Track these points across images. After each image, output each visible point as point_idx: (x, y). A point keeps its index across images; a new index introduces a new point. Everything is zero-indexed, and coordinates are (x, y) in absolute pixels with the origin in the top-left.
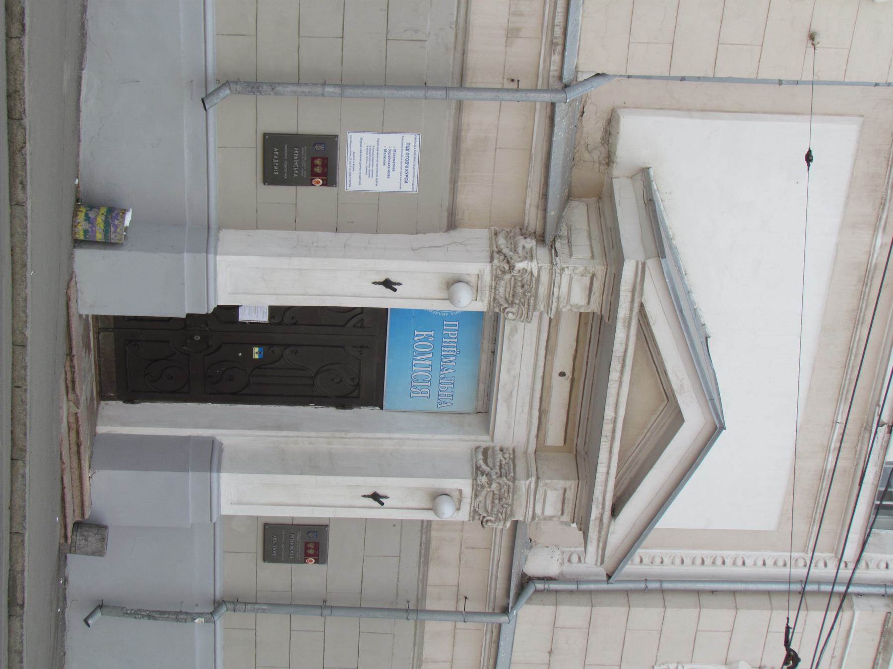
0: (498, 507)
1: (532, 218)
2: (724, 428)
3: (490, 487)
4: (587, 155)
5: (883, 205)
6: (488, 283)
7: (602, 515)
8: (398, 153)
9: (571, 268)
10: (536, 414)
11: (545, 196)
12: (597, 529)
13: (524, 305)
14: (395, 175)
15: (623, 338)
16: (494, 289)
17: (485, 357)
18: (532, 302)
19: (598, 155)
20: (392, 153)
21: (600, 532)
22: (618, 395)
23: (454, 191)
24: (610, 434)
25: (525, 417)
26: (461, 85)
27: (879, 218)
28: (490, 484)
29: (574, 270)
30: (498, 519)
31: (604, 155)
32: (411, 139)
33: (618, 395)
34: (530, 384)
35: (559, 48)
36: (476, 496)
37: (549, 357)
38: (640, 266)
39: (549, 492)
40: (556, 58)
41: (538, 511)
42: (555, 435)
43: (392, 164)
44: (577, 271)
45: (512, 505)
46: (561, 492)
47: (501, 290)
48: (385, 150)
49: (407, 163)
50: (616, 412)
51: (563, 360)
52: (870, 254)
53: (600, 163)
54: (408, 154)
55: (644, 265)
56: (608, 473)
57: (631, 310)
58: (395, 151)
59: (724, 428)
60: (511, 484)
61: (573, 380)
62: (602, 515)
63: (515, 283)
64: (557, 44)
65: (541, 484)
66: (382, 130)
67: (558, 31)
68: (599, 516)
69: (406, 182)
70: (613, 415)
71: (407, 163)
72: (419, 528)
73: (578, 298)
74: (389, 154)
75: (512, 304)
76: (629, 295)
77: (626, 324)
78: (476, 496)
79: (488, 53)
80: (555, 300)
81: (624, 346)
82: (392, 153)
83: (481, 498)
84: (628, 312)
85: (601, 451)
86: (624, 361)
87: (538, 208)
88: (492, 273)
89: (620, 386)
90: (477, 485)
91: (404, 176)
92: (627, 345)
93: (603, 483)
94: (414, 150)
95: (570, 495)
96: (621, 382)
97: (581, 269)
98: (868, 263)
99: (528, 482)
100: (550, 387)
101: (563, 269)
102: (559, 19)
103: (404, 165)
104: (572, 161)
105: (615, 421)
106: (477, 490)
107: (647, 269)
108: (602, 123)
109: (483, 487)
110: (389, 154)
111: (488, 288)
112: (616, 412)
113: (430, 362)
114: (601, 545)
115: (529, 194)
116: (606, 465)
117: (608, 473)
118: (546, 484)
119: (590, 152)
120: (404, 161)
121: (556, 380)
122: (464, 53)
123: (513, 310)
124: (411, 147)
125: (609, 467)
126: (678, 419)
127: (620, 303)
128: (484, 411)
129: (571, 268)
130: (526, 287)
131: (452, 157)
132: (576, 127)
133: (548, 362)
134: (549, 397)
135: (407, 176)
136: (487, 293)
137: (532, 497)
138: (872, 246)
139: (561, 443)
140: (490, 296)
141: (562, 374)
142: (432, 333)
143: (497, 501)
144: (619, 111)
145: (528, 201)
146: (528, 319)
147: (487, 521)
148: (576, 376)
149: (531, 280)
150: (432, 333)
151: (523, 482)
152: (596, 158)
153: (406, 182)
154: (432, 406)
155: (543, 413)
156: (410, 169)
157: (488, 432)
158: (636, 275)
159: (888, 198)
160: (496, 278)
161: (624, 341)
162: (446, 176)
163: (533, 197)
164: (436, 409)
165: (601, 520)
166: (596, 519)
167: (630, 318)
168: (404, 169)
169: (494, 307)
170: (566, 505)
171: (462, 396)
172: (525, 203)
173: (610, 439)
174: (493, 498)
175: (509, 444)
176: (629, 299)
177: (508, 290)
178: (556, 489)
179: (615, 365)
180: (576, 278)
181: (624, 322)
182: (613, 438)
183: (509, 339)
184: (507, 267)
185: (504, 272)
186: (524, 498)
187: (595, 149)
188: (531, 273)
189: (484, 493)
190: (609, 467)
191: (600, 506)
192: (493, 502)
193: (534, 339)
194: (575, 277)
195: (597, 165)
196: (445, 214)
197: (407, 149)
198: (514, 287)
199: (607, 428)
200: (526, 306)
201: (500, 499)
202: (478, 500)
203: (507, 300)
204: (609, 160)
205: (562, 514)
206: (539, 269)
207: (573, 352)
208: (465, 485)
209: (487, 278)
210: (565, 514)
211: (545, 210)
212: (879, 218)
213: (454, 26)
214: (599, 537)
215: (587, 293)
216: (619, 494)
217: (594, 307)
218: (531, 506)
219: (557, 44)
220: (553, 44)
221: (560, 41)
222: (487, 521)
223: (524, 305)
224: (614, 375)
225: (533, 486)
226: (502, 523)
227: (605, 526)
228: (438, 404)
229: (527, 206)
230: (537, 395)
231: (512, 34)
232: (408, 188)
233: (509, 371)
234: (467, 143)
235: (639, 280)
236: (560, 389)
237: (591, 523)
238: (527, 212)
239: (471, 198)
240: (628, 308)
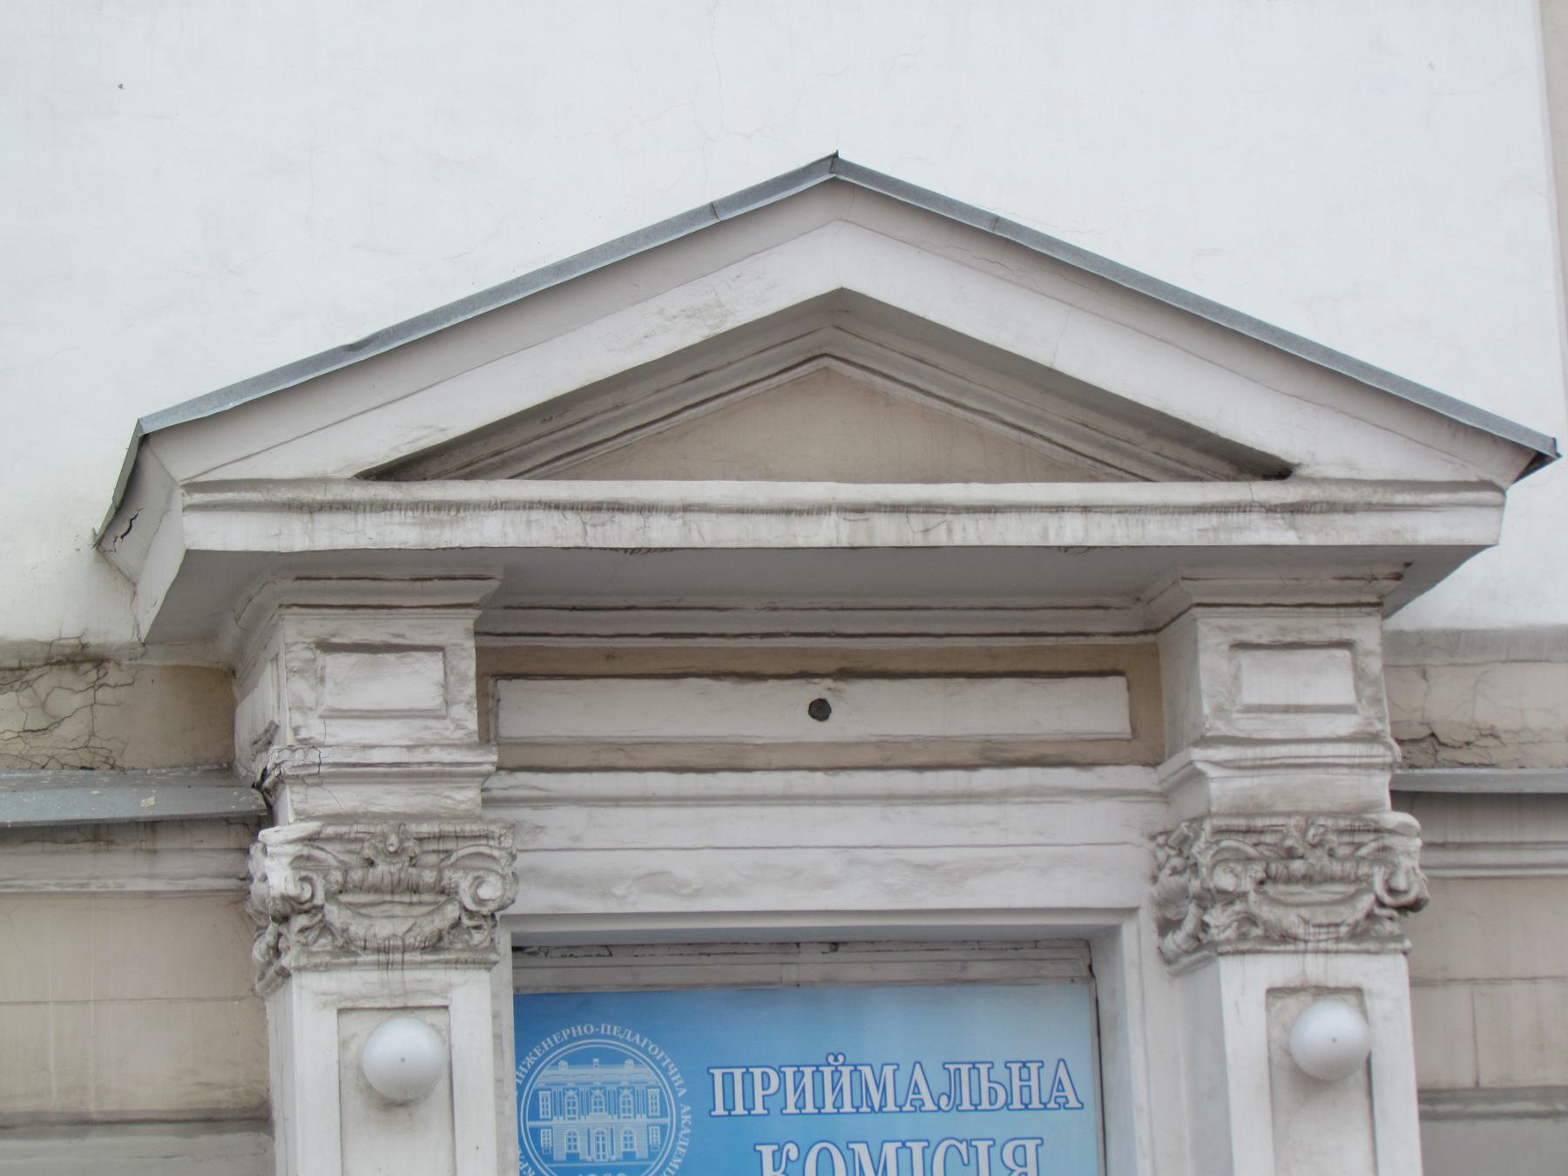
0: (1318, 859)
1: (189, 867)
2: (836, 156)
3: (1243, 896)
4: (68, 730)
6: (374, 976)
7: (1271, 509)
9: (298, 719)
10: (987, 779)
11: (98, 834)
12: (1341, 519)
13: (448, 853)
15: (504, 519)
16: (387, 953)
17: (853, 967)
18: (426, 828)
19: (67, 696)
21: (1349, 509)
22: (742, 511)
24: (916, 521)
25: (1015, 813)
28: (1229, 898)
29: (301, 708)
30: (1384, 855)
31: (67, 677)
33: (742, 511)
34: (875, 811)
36: (1286, 937)
37: (760, 758)
38: (198, 498)
39: (1250, 697)
41: (1344, 725)
42: (1097, 708)
44: (309, 700)
45: (1310, 818)
46: (1245, 658)
50: (821, 510)
51: (775, 714)
53: (98, 685)
55: (192, 487)
56: (1086, 509)
57: (385, 506)
59: (836, 156)
60: (1208, 826)
61: (846, 674)
62: (1271, 509)
63: (359, 888)
65: (1222, 728)
68: (1279, 519)
70: (831, 520)
72: (1547, 1124)
73: (414, 683)
75: (446, 892)
76: (324, 520)
77: (444, 516)
78: (1286, 937)
80: (418, 756)
81: (536, 515)
83: (1290, 920)
84: (397, 517)
85: (995, 540)
86: (596, 507)
87: (154, 852)
88: (328, 967)
89: (705, 509)
90: (1243, 937)
92: (530, 505)
93: (1133, 519)
95: (1260, 627)
96: (687, 508)
97: (300, 687)
99: (1212, 772)
100: (881, 744)
101: (308, 744)
105: (859, 509)
106: (1267, 938)
109: (1251, 920)
111: (394, 976)
112: (821, 510)
113: (890, 1149)
114: (1407, 498)
115: (112, 885)
116: (1052, 521)
117: (1086, 509)
118: (1220, 711)
119: (58, 722)
121: (840, 728)
123: (465, 885)
125: (1059, 509)
126: (841, 307)
127: (363, 543)
128: (1070, 954)
129: (298, 719)
130: (368, 852)
133: (777, 759)
134: (925, 742)
136: (411, 975)
137: (1271, 751)
139: (1115, 687)
140: (422, 965)
141: (820, 710)
142: (767, 1151)
143: (1297, 866)
145: (142, 885)
147: (1392, 891)
148: (833, 666)
149: (339, 838)
150: (767, 1151)
151: (1214, 788)
152: (77, 701)
154: (1078, 1127)
155: (995, 755)
157: (1112, 933)
158: (243, 507)
160: (347, 950)
161: (521, 516)
163: (122, 870)
164: (1091, 1113)
165: (1295, 509)
166: (1293, 527)
167: (416, 506)
170: (1307, 637)
171: (1013, 1033)
172: (151, 895)
173: (933, 519)
174: (1290, 880)
175: (1138, 857)
176: (342, 520)
177: (398, 910)
178: (1236, 677)
179: (622, 533)
181: (441, 523)
182: (929, 508)
183: (696, 894)
184: (301, 921)
185: (326, 928)
186: (1280, 778)
187: (43, 706)
188: (311, 839)
189: (1267, 912)
190: (1059, 509)
191: (1235, 519)
192: (1307, 879)
193: (687, 813)
194: (330, 701)
198: (376, 889)
199: (887, 532)
200: (450, 845)
201: (1291, 854)
202: (1300, 931)
204: (79, 658)
205: (1346, 645)
207: (726, 686)
208: (1243, 983)
209: (354, 981)
210: (1346, 635)
211: (152, 826)
214: (1370, 507)
215: (390, 657)
216: (1227, 469)
217: (457, 633)
218: (1328, 749)
222: (1392, 891)
223: (448, 853)
224: (663, 533)
225: (1225, 753)
226: (1390, 840)
227: (1314, 493)
228: (1063, 1106)
229: (158, 886)
230: (819, 782)
233: (829, 883)
235: (254, 496)
236: (868, 712)
237: (1312, 540)
238: (182, 885)
240: (383, 517)
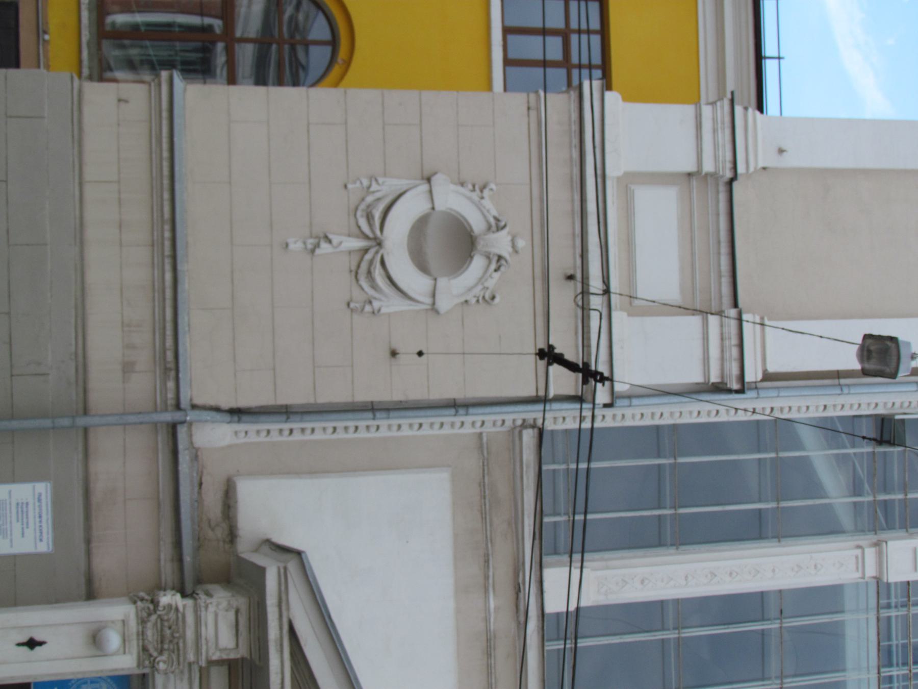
1: (168, 571)
5: (487, 562)
8: (31, 507)
9: (215, 604)
14: (29, 532)
16: (142, 634)
18: (181, 645)
19: (220, 532)
20: (25, 506)
23: (89, 553)
26: (86, 412)
27: (486, 577)
32: (43, 488)
35: (173, 374)
38: (282, 571)
40: (171, 384)
43: (25, 520)
44: (221, 607)
47: (149, 633)
48: (18, 504)
49: (40, 517)
52: (487, 620)
53: (224, 541)
54: (40, 507)
55: (285, 569)
57: (281, 628)
58: (27, 504)
63: (162, 625)
64: (170, 370)
66: (13, 480)
67: (170, 355)
69: (41, 540)
71: (40, 517)
73: (226, 639)
74: (22, 507)
75: (161, 652)
76: (276, 610)
79: (106, 387)
80: (204, 642)
82: (25, 506)
84: (278, 632)
91: (38, 534)
94: (47, 501)
97: (224, 604)
98: (488, 630)
102: (169, 342)
103: (38, 520)
104: (200, 543)
107: (289, 575)
108: (220, 495)
110: (22, 508)
119: (213, 530)
120: (37, 516)
122: (85, 391)
124: (43, 497)
130: (173, 627)
131: (81, 511)
132: (199, 502)
135: (41, 533)
136: (135, 643)
138: (487, 609)
140: (138, 645)
144: (235, 479)
146: (182, 680)
149: (177, 618)
153: (41, 540)
156: (44, 524)
158: (280, 584)
159: (490, 552)
160: (143, 622)
161: (279, 670)
162: (79, 534)
163: (166, 552)
168: (38, 524)
169: (144, 661)
176: (276, 615)
180: (221, 614)
188: (177, 609)
195: (221, 544)
196: (83, 580)
197: (40, 500)
198: (162, 630)
203: (156, 649)
204: (232, 535)
206: (184, 606)
212: (486, 577)
213: (73, 357)
217: (243, 652)
219: (170, 370)
220: (166, 370)
221: (171, 365)
229: (162, 563)
231: (128, 368)
232: (44, 547)
234: (99, 487)
235: (283, 588)
238: (163, 570)
239: (107, 562)
240: (278, 627)
